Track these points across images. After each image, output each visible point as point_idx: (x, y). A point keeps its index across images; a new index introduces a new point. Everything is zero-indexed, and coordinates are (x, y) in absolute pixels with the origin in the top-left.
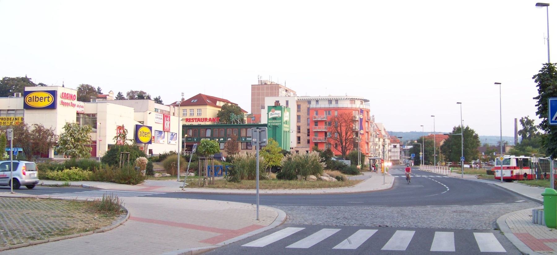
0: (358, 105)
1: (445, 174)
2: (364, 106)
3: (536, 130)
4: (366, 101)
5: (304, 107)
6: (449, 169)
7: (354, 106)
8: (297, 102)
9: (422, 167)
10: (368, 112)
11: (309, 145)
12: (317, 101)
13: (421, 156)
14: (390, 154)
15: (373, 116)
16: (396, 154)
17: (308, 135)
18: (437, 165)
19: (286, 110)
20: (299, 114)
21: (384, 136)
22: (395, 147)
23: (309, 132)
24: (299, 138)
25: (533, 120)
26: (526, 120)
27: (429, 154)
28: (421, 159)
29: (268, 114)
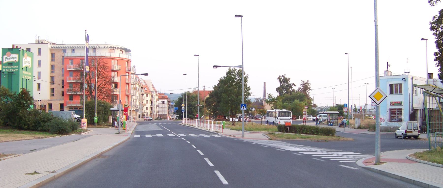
0: (118, 54)
1: (212, 130)
2: (125, 56)
3: (291, 88)
4: (127, 51)
5: (59, 56)
6: (215, 123)
7: (113, 55)
8: (51, 50)
9: (185, 122)
10: (129, 62)
11: (63, 97)
12: (73, 50)
13: (183, 108)
14: (158, 109)
15: (134, 67)
16: (164, 109)
17: (63, 87)
18: (201, 118)
19: (25, 54)
20: (53, 63)
21: (152, 92)
22: (163, 102)
23: (63, 84)
24: (53, 90)
25: (290, 79)
26: (283, 78)
27: (194, 109)
28: (183, 112)
29: (2, 58)
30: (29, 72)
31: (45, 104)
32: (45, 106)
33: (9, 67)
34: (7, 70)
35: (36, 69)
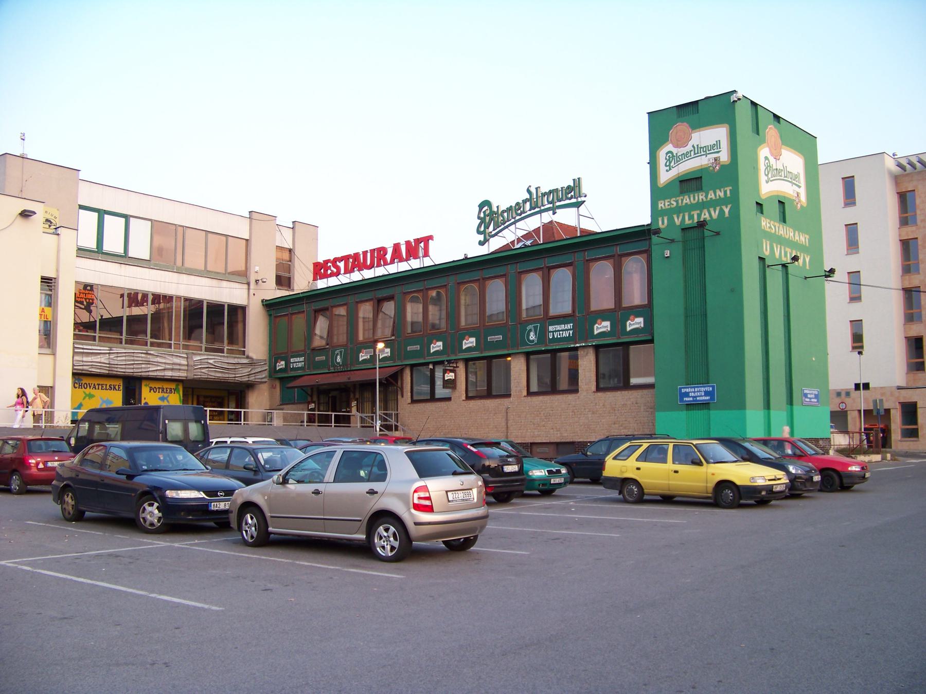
8: (897, 179)
30: (796, 228)
31: (886, 406)
32: (888, 411)
33: (686, 200)
34: (677, 221)
35: (833, 218)
